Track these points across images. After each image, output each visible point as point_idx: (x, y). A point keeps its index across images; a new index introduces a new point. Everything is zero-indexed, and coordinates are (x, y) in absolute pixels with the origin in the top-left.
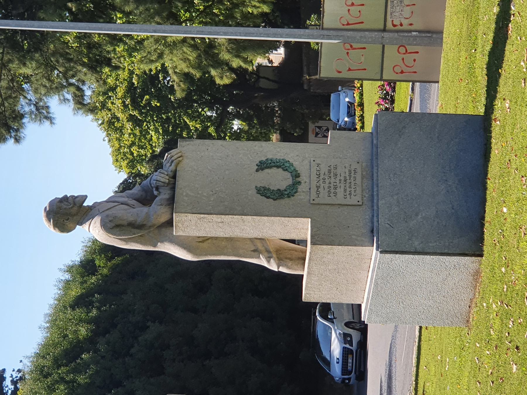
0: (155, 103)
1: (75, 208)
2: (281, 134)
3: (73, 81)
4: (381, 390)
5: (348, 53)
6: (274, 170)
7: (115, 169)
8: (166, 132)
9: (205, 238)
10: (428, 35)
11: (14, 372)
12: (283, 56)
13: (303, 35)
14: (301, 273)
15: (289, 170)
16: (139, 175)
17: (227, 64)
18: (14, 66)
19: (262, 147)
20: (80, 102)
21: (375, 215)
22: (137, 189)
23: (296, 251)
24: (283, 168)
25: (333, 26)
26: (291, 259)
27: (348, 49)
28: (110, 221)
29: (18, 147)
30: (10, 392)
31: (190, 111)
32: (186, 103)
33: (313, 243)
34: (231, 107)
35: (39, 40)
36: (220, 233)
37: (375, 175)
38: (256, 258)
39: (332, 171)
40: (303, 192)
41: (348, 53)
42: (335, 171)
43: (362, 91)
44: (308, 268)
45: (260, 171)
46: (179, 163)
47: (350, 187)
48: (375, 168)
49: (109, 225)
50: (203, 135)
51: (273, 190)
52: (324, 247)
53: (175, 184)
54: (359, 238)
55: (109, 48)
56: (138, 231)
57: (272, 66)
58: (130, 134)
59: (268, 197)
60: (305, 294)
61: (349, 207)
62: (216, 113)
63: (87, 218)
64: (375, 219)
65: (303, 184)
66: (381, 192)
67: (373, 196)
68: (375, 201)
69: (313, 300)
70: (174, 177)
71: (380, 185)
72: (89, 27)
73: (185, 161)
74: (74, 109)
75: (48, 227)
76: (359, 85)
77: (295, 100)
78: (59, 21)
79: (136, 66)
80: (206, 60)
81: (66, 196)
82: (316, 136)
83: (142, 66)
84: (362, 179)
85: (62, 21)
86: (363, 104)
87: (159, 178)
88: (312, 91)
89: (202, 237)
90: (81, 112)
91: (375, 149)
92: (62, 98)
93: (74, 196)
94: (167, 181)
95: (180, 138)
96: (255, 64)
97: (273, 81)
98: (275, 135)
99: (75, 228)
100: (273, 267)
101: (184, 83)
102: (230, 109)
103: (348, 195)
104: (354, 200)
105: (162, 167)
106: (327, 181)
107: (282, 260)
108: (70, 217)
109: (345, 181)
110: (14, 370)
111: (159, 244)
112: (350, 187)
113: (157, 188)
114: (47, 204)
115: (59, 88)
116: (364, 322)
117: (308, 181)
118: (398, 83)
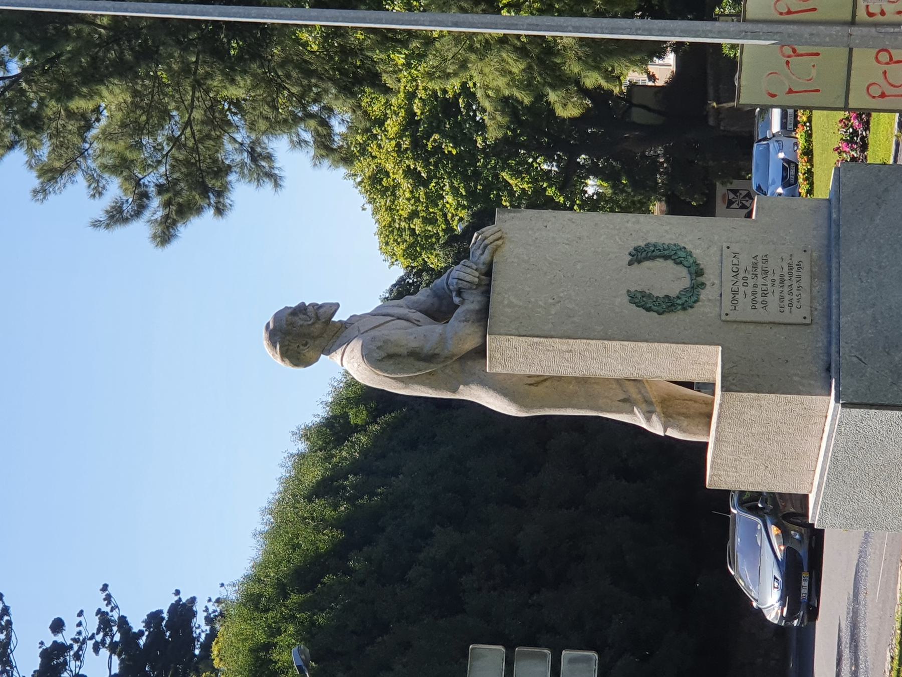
0: (449, 148)
1: (318, 325)
2: (668, 203)
3: (315, 108)
4: (839, 645)
5: (788, 63)
6: (660, 263)
7: (383, 257)
8: (472, 196)
9: (542, 378)
11: (211, 603)
15: (685, 263)
16: (425, 268)
17: (577, 82)
18: (216, 83)
19: (638, 222)
20: (325, 146)
21: (834, 341)
22: (423, 295)
23: (695, 402)
24: (674, 260)
25: (761, 16)
26: (687, 416)
27: (789, 56)
28: (378, 348)
29: (221, 222)
30: (203, 636)
31: (512, 162)
32: (505, 150)
33: (725, 388)
34: (583, 156)
35: (257, 38)
36: (565, 369)
37: (834, 272)
38: (627, 413)
39: (760, 264)
40: (709, 300)
41: (788, 63)
42: (764, 265)
43: (811, 130)
44: (717, 431)
45: (636, 264)
46: (496, 250)
47: (791, 293)
48: (834, 260)
50: (538, 201)
51: (657, 297)
52: (745, 395)
53: (489, 285)
54: (805, 381)
55: (378, 55)
57: (655, 87)
58: (409, 200)
59: (648, 310)
60: (711, 476)
61: (789, 327)
62: (558, 166)
63: (338, 343)
64: (834, 348)
66: (845, 301)
67: (829, 307)
68: (834, 317)
69: (724, 487)
70: (488, 273)
71: (842, 289)
74: (315, 157)
75: (272, 358)
76: (805, 119)
77: (691, 147)
78: (293, 7)
79: (408, 82)
80: (540, 75)
81: (303, 303)
82: (728, 207)
83: (430, 85)
84: (812, 278)
85: (297, 7)
86: (812, 151)
87: (462, 275)
88: (722, 128)
89: (534, 376)
90: (326, 162)
91: (834, 228)
92: (295, 139)
93: (317, 305)
94: (476, 280)
95: (499, 207)
96: (626, 82)
97: (653, 111)
98: (657, 204)
99: (317, 360)
100: (657, 429)
101: (503, 113)
102: (582, 159)
103: (786, 307)
104: (796, 316)
105: (467, 257)
106: (751, 282)
107: (671, 417)
108: (309, 341)
109: (782, 281)
110: (210, 600)
111: (461, 387)
112: (791, 293)
113: (459, 293)
114: (270, 318)
115: (288, 124)
116: (813, 524)
117: (717, 282)
118: (874, 114)
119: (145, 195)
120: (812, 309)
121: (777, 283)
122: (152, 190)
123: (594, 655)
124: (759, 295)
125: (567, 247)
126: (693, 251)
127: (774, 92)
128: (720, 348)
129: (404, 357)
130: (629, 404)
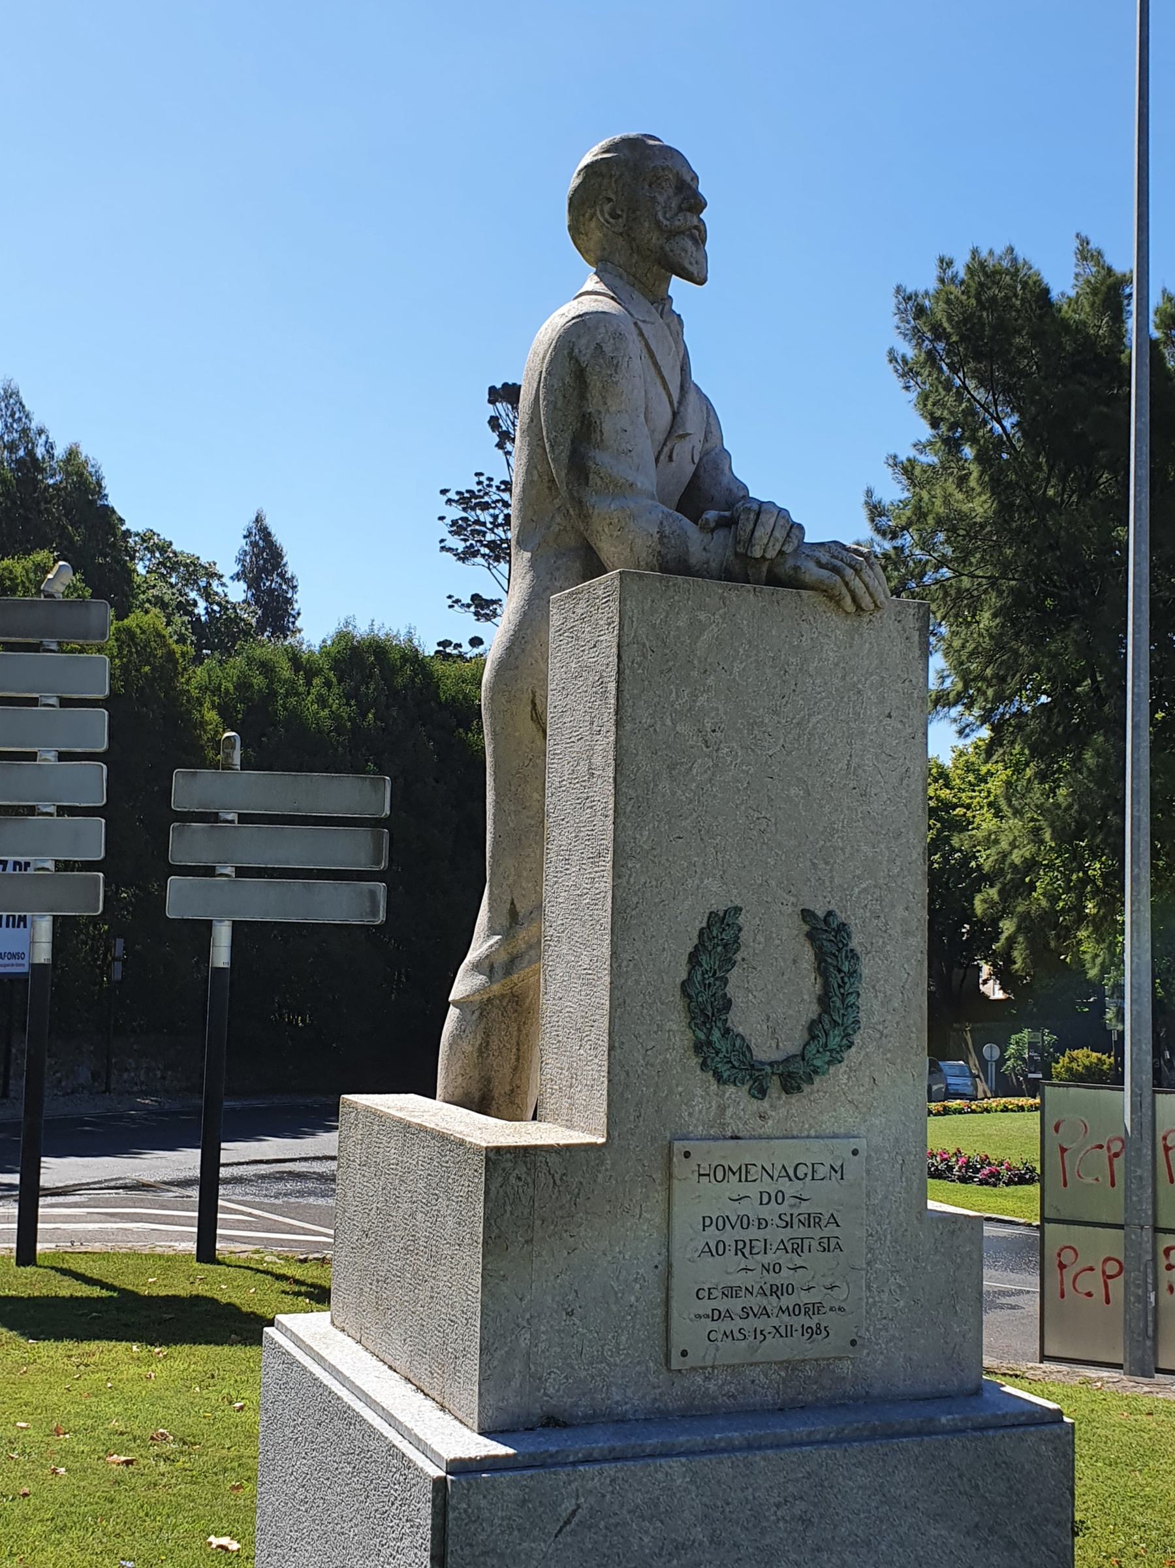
1: (655, 239)
5: (1101, 1147)
6: (810, 985)
10: (1150, 1330)
12: (992, 997)
13: (1140, 1049)
14: (439, 1091)
15: (812, 1048)
19: (907, 933)
23: (515, 1069)
26: (483, 1050)
27: (1109, 1149)
28: (599, 346)
39: (816, 1233)
40: (722, 1109)
42: (815, 1244)
46: (831, 598)
47: (746, 1313)
49: (583, 341)
51: (725, 981)
52: (480, 1209)
54: (518, 1366)
56: (565, 456)
63: (618, 282)
64: (601, 1442)
65: (755, 1105)
66: (724, 1468)
71: (757, 1457)
72: (1140, 586)
73: (836, 625)
84: (787, 1364)
94: (758, 554)
100: (464, 984)
103: (713, 1304)
104: (689, 1331)
106: (770, 1212)
109: (776, 1291)
111: (528, 555)
112: (746, 1313)
117: (769, 1127)
119: (894, 536)
120: (708, 1371)
121: (772, 1278)
122: (899, 542)
123: (382, 917)
124: (739, 1234)
125: (843, 765)
126: (843, 1067)
127: (1061, 1129)
128: (602, 1140)
129: (580, 407)
130: (506, 923)
